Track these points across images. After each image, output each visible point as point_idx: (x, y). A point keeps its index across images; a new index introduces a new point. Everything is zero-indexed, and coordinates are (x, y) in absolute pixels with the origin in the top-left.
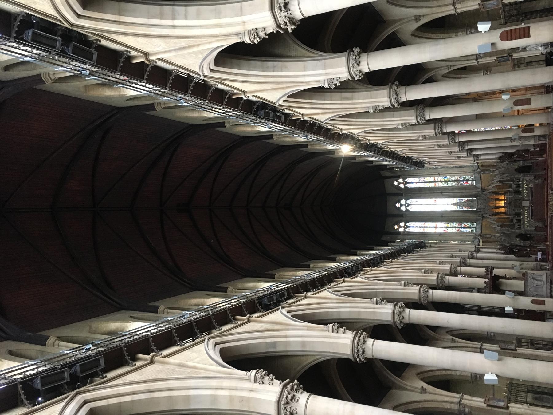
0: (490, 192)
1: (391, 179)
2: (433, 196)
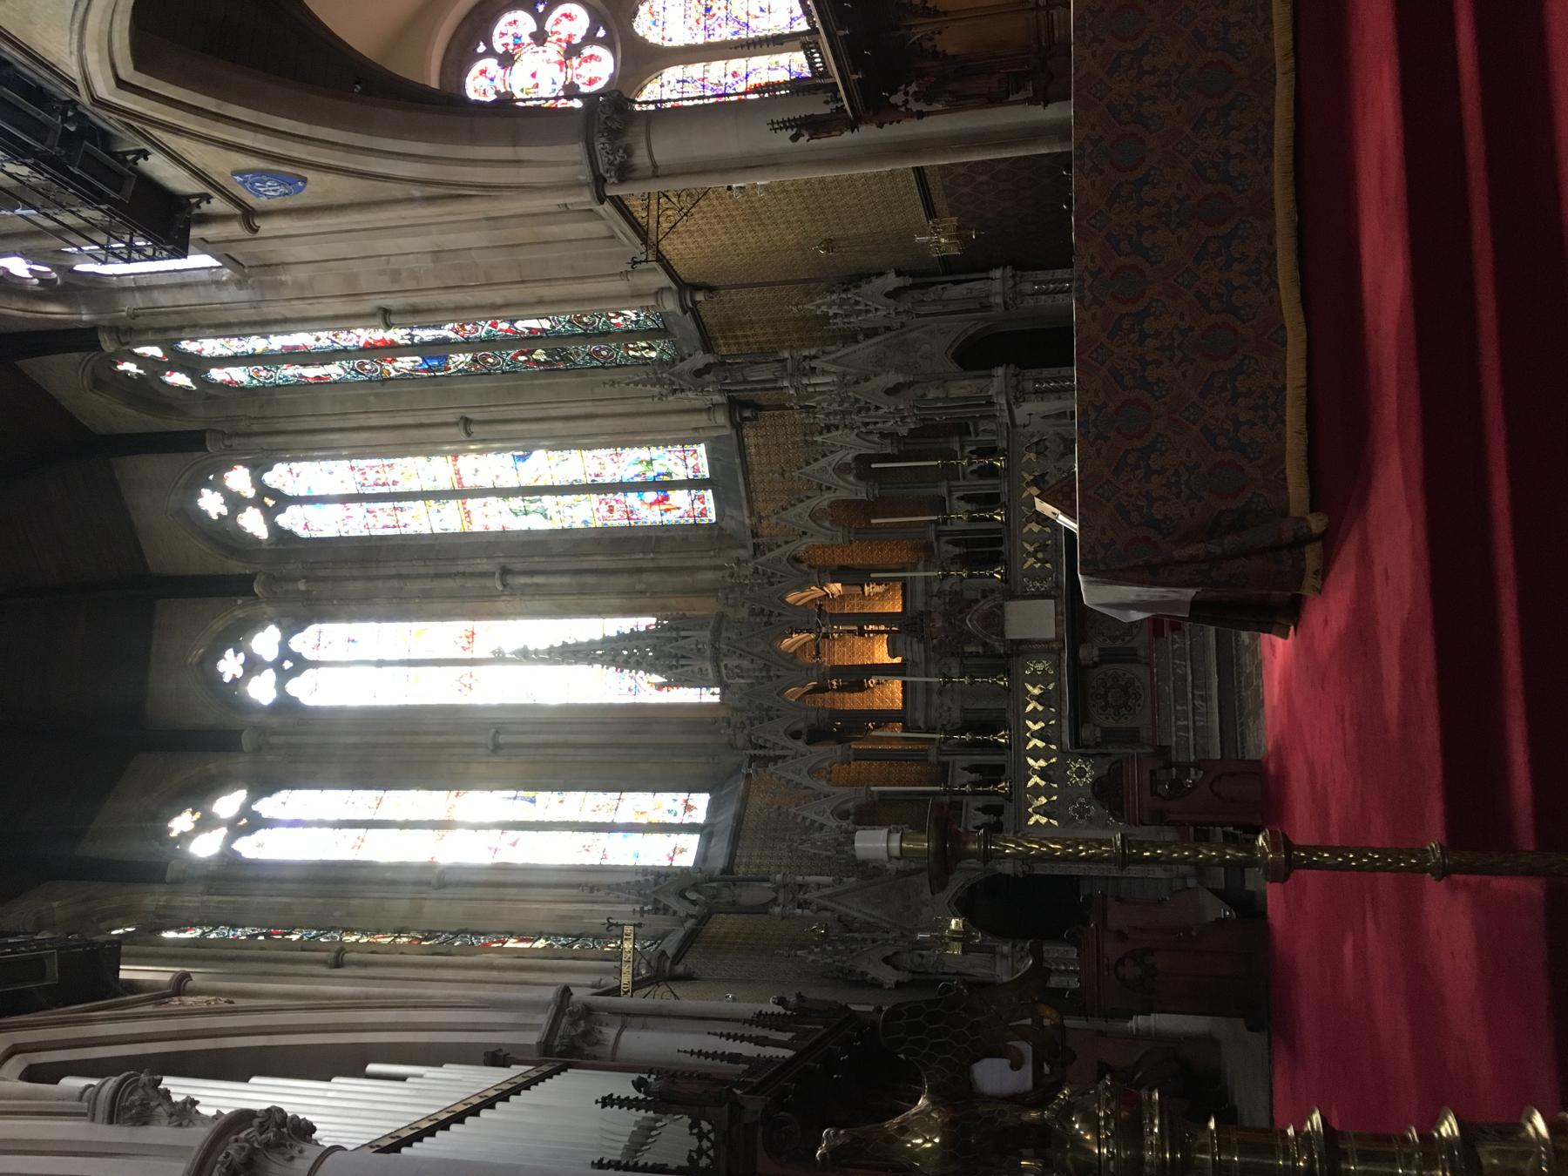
1: (152, 466)
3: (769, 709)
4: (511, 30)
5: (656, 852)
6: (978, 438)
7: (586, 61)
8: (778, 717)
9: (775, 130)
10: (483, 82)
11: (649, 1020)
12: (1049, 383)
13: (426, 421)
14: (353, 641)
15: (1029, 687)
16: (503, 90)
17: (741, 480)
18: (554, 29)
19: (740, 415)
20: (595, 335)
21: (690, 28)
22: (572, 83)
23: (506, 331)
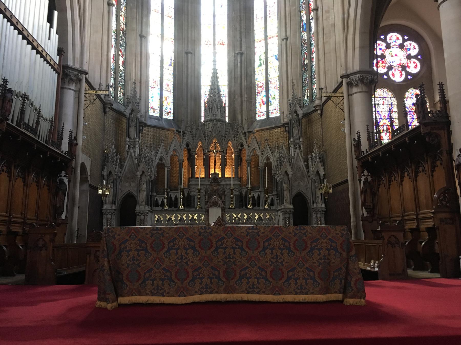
0: (242, 145)
2: (234, 37)
3: (195, 137)
4: (412, 47)
5: (154, 103)
6: (276, 200)
7: (400, 73)
8: (193, 140)
9: (357, 133)
10: (394, 38)
11: (77, 99)
12: (288, 222)
13: (287, 26)
14: (221, 7)
15: (196, 215)
16: (391, 45)
17: (268, 127)
18: (412, 62)
19: (286, 126)
20: (312, 79)
21: (410, 107)
22: (393, 68)
23: (313, 50)
